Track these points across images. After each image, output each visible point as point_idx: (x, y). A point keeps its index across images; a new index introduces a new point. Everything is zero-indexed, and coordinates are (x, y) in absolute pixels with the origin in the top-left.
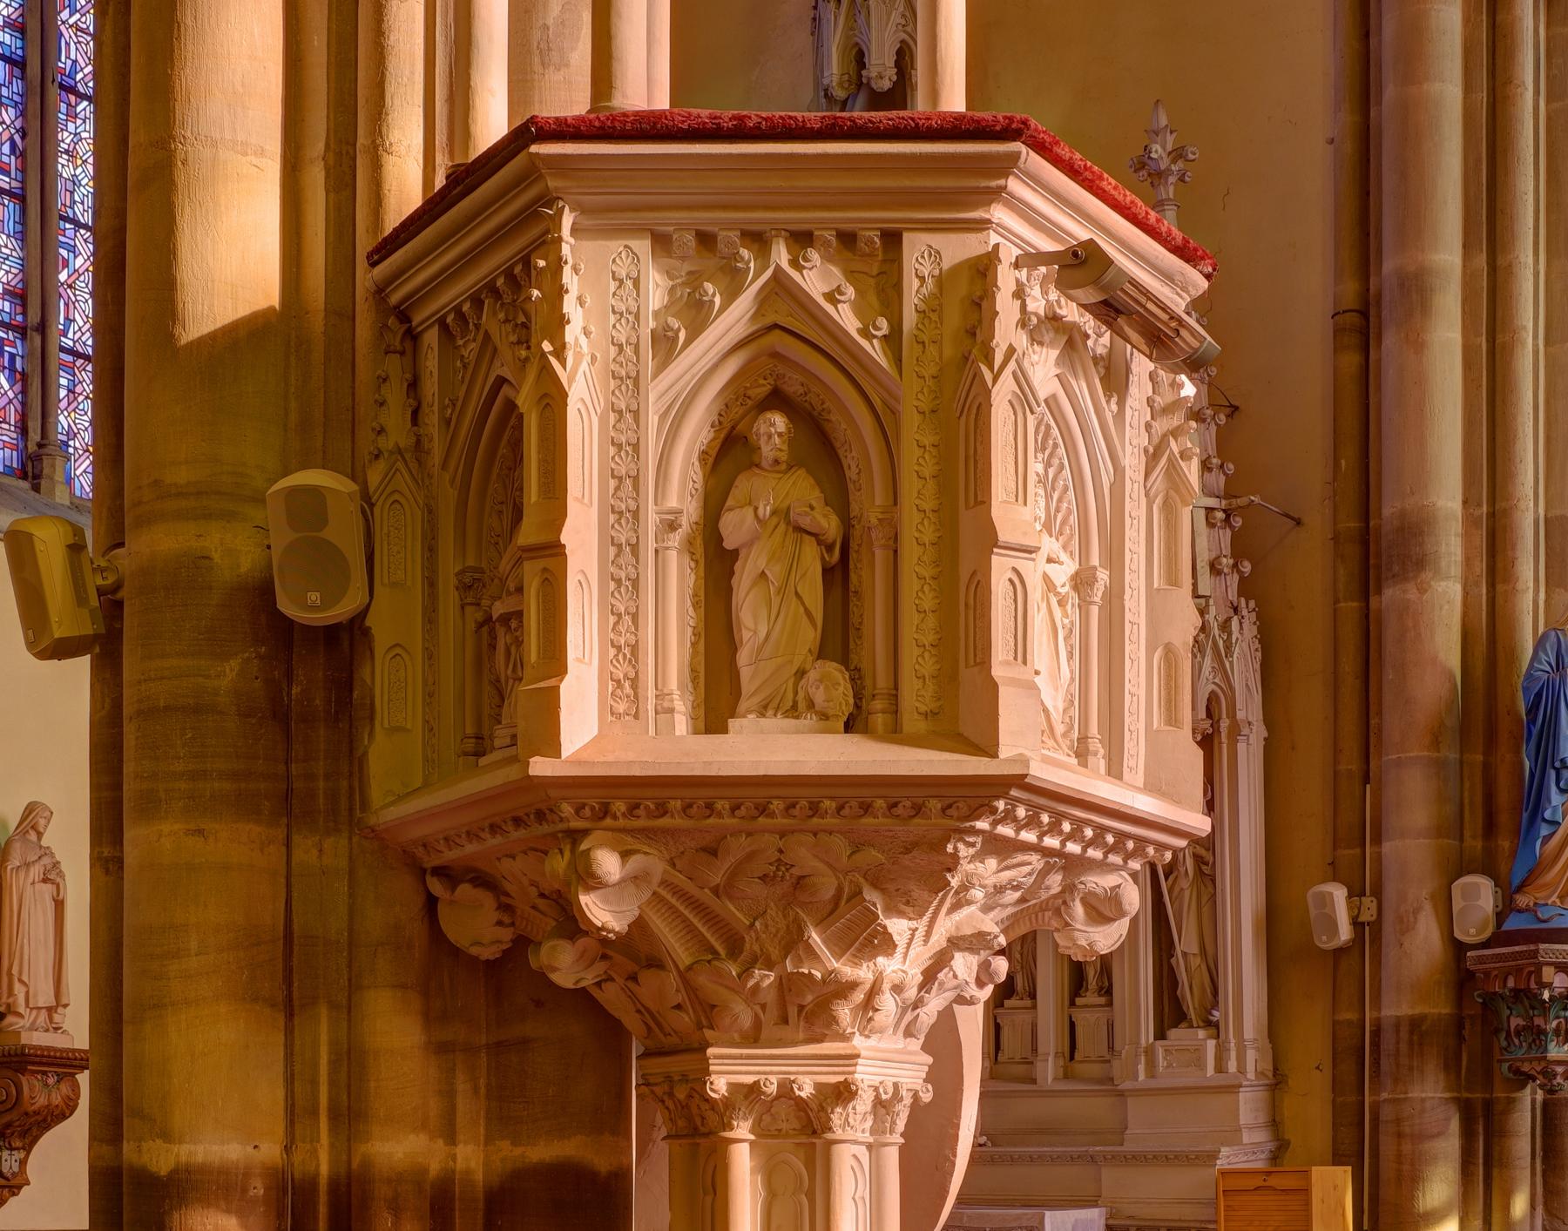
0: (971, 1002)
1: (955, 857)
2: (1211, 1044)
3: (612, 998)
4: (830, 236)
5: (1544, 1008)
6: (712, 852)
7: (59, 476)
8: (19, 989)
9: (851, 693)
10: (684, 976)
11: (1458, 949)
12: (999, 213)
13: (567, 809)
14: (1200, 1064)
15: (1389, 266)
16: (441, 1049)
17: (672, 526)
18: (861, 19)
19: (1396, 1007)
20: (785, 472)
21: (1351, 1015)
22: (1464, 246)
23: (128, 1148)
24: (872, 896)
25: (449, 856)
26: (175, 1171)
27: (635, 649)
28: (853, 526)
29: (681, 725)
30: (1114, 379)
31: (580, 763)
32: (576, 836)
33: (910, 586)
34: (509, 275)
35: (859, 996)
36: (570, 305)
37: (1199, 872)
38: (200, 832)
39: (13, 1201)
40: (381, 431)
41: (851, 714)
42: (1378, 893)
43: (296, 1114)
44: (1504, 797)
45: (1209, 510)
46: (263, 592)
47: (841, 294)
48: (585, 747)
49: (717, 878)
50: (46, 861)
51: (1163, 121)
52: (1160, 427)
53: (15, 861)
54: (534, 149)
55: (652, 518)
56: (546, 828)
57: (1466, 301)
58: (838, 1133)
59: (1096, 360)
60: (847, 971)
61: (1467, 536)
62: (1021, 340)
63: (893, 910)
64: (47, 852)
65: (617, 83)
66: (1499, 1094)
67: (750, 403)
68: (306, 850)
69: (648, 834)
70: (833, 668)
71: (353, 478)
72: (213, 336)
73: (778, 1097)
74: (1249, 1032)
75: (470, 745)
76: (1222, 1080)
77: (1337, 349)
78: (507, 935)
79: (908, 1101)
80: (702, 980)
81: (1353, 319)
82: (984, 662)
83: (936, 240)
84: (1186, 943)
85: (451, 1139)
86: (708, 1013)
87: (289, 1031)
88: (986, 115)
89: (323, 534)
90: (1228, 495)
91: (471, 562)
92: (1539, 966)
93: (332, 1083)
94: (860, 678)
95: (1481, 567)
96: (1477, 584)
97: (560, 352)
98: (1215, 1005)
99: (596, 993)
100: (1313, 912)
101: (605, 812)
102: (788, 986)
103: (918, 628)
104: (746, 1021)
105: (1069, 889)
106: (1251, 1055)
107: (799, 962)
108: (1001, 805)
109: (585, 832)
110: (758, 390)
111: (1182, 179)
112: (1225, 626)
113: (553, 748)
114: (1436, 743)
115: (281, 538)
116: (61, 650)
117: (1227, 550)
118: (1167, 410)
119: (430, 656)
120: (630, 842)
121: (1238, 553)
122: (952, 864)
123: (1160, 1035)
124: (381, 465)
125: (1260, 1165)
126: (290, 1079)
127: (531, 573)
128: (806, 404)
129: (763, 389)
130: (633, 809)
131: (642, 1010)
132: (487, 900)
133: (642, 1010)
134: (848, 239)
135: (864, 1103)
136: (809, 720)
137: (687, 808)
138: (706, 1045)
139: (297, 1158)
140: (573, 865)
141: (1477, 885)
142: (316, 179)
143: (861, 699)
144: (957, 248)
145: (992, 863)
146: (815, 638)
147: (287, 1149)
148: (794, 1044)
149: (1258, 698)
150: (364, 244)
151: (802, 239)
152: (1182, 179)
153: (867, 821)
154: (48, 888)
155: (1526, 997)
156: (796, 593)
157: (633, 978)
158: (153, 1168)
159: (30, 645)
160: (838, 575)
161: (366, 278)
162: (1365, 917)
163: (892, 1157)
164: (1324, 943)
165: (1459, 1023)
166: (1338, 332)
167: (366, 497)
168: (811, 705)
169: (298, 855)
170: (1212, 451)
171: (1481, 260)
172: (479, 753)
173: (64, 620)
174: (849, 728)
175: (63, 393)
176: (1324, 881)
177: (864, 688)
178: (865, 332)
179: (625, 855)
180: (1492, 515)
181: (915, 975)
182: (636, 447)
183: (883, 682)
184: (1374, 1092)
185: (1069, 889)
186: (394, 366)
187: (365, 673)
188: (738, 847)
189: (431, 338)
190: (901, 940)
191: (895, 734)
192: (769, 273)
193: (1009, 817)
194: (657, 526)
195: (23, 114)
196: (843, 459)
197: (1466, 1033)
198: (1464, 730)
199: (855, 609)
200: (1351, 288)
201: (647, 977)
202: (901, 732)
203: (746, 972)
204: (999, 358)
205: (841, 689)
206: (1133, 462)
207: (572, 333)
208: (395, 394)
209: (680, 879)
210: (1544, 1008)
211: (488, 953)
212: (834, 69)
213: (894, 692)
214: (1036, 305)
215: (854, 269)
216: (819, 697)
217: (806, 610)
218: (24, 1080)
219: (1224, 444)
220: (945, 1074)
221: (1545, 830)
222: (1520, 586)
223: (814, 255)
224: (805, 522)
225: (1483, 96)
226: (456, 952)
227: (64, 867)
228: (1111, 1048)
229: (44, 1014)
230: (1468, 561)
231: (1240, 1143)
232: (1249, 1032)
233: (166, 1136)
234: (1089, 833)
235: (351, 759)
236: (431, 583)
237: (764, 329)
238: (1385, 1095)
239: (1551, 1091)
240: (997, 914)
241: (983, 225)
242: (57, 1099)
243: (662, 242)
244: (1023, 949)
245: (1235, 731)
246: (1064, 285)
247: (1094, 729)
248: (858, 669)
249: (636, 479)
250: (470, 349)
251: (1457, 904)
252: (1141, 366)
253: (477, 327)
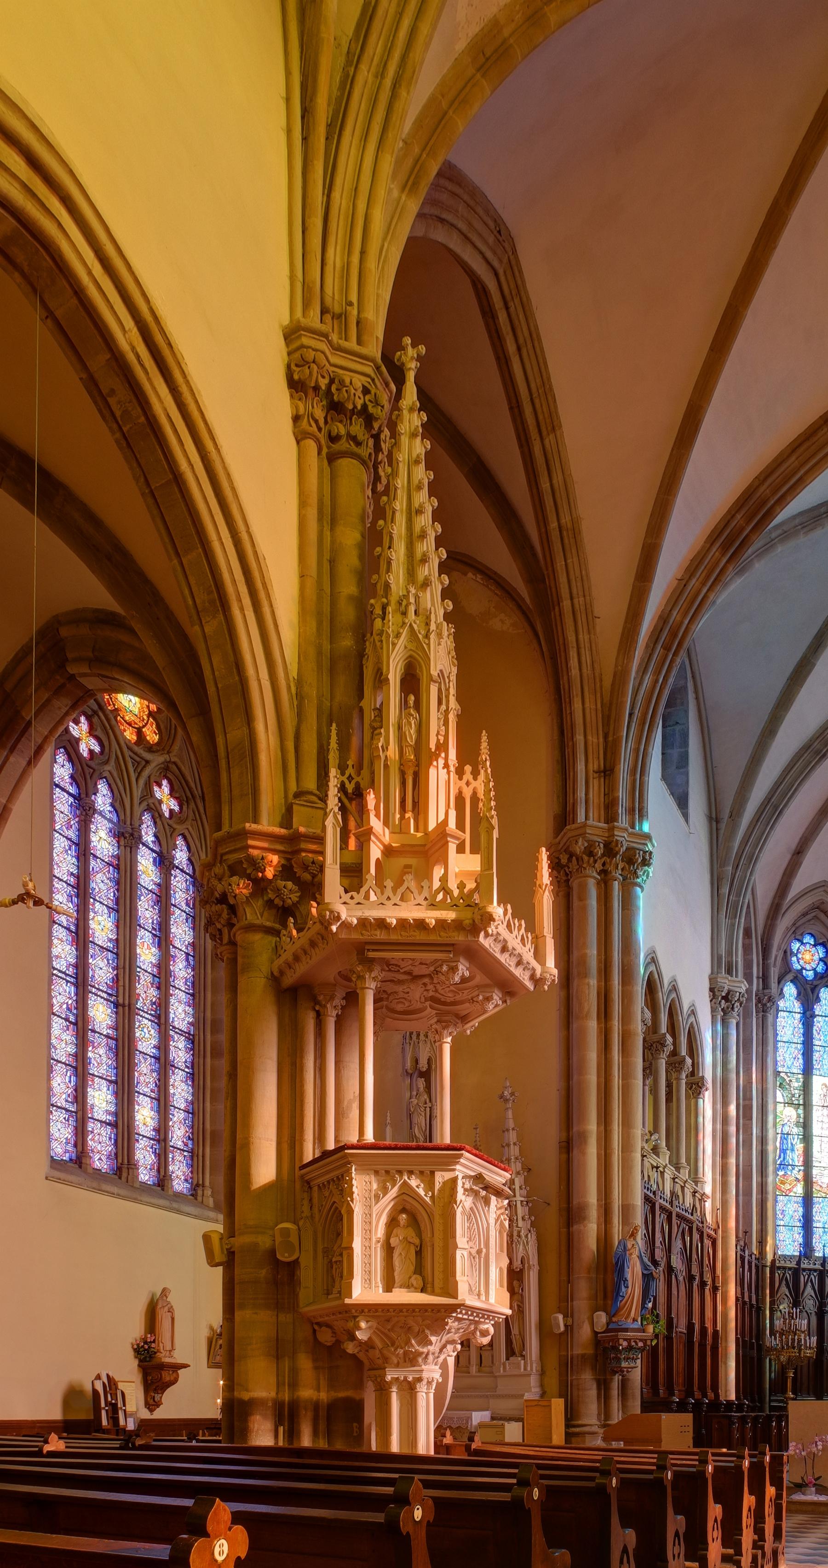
0: (451, 1356)
1: (448, 1322)
2: (522, 1362)
3: (361, 1356)
4: (418, 1172)
5: (620, 1352)
6: (388, 1321)
7: (170, 1186)
8: (161, 1345)
10: (380, 1351)
11: (596, 1333)
12: (458, 1167)
13: (353, 1311)
14: (519, 1368)
15: (575, 1129)
16: (316, 1368)
17: (379, 1242)
18: (417, 1049)
19: (578, 1351)
21: (564, 1353)
22: (598, 1123)
23: (235, 1393)
24: (427, 1332)
25: (320, 1320)
26: (249, 1400)
27: (370, 1272)
29: (381, 1290)
30: (487, 1202)
31: (357, 1300)
32: (355, 1317)
33: (436, 1257)
34: (338, 1177)
35: (424, 1356)
36: (354, 1189)
38: (256, 1313)
39: (158, 1409)
40: (303, 1212)
42: (572, 1316)
43: (279, 1385)
44: (609, 1288)
45: (522, 1201)
46: (272, 1253)
49: (389, 1327)
50: (169, 1305)
51: (508, 1084)
52: (499, 1212)
53: (160, 1306)
54: (346, 1151)
55: (374, 1240)
56: (347, 1315)
57: (598, 1140)
58: (418, 1390)
59: (482, 1197)
60: (421, 1350)
61: (598, 1210)
62: (463, 1198)
63: (432, 1335)
64: (169, 1303)
65: (365, 1133)
66: (608, 1377)
68: (282, 1317)
69: (373, 1317)
70: (419, 1277)
71: (294, 1223)
72: (260, 1188)
73: (403, 1381)
74: (534, 1358)
75: (326, 1292)
76: (526, 1372)
77: (560, 1153)
78: (334, 1339)
79: (435, 1381)
80: (385, 1352)
81: (564, 1144)
82: (454, 1237)
83: (443, 1173)
85: (319, 1391)
86: (386, 1360)
87: (277, 1364)
88: (455, 1144)
89: (290, 1239)
90: (527, 1197)
91: (326, 1246)
92: (619, 1339)
93: (289, 1377)
95: (602, 1219)
97: (352, 1200)
98: (524, 1350)
99: (357, 1355)
100: (553, 1322)
101: (363, 1311)
102: (406, 1353)
103: (438, 1268)
104: (396, 1361)
105: (476, 1329)
106: (534, 1365)
107: (409, 1348)
108: (459, 1310)
109: (358, 1316)
111: (514, 1101)
112: (526, 1236)
113: (350, 1297)
114: (589, 1272)
115: (278, 1240)
116: (217, 1265)
117: (527, 1214)
118: (500, 1208)
119: (315, 1269)
120: (369, 1319)
121: (530, 1215)
122: (447, 1324)
123: (507, 1359)
124: (303, 1220)
125: (537, 1398)
126: (278, 1376)
127: (345, 1253)
129: (401, 1207)
130: (369, 1311)
131: (369, 1359)
132: (329, 1331)
133: (369, 1359)
134: (422, 1173)
135: (425, 1382)
136: (412, 1289)
137: (383, 1310)
138: (385, 1368)
139: (280, 1396)
140: (354, 1324)
141: (601, 1315)
142: (285, 1146)
144: (448, 1175)
145: (456, 1323)
148: (407, 1367)
149: (536, 1257)
150: (298, 1165)
151: (411, 1173)
152: (514, 1101)
153: (426, 1314)
154: (170, 1313)
155: (615, 1348)
157: (367, 1351)
158: (244, 1398)
159: (209, 1263)
160: (419, 1253)
161: (298, 1173)
163: (431, 1396)
164: (556, 1331)
165: (596, 1356)
166: (560, 1148)
167: (299, 1229)
168: (413, 1285)
169: (280, 1318)
170: (523, 1183)
171: (602, 1128)
172: (328, 1294)
173: (219, 1257)
174: (422, 1291)
175: (170, 1159)
176: (557, 1313)
178: (426, 1195)
179: (367, 1322)
180: (605, 1204)
181: (438, 1350)
182: (370, 1223)
183: (430, 1279)
184: (572, 1376)
185: (476, 1329)
186: (306, 1195)
187: (298, 1273)
188: (395, 1319)
189: (316, 1189)
190: (434, 1342)
191: (433, 1293)
193: (461, 1313)
195: (159, 1074)
197: (598, 1358)
200: (564, 1134)
201: (370, 1350)
203: (396, 1349)
204: (458, 1203)
206: (492, 1221)
207: (355, 1196)
208: (306, 1202)
209: (380, 1327)
210: (620, 1352)
211: (329, 1344)
212: (409, 1064)
214: (467, 1186)
216: (415, 1283)
218: (163, 1372)
219: (526, 1181)
220: (445, 1375)
221: (620, 1299)
222: (614, 1225)
223: (413, 1176)
224: (411, 1241)
225: (603, 1080)
226: (320, 1343)
227: (174, 1307)
228: (493, 1362)
229: (168, 1352)
230: (598, 1218)
231: (531, 1391)
232: (534, 1358)
233: (247, 1390)
234: (481, 1315)
235: (294, 1295)
236: (315, 1251)
237: (401, 1194)
238: (574, 1377)
239: (623, 1376)
240: (457, 1335)
241: (454, 1170)
242: (172, 1378)
243: (376, 1173)
244: (466, 1344)
245: (529, 1267)
246: (475, 1183)
250: (327, 1194)
251: (595, 1320)
252: (493, 1198)
253: (329, 1188)
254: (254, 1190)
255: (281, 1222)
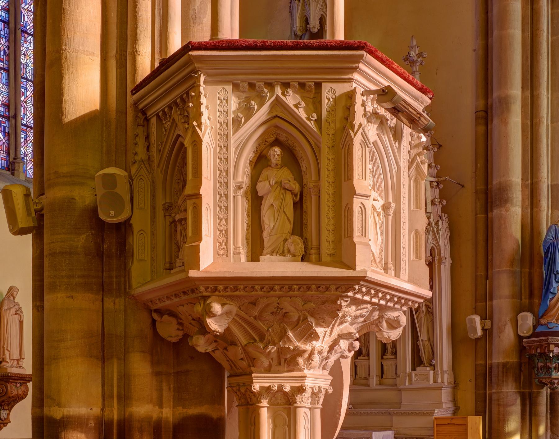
0: (346, 357)
1: (341, 306)
2: (432, 372)
3: (218, 356)
4: (296, 84)
5: (550, 359)
6: (254, 304)
7: (21, 170)
8: (7, 353)
9: (303, 247)
10: (244, 348)
11: (520, 338)
12: (356, 76)
13: (202, 289)
14: (428, 379)
15: (495, 95)
16: (157, 374)
17: (240, 188)
18: (307, 7)
19: (498, 359)
20: (280, 168)
21: (481, 362)
22: (522, 88)
23: (45, 409)
24: (311, 320)
25: (160, 305)
26: (62, 418)
27: (226, 231)
28: (304, 188)
29: (243, 258)
30: (397, 135)
31: (207, 272)
32: (205, 298)
33: (324, 209)
34: (182, 98)
35: (306, 355)
36: (203, 109)
37: (428, 311)
38: (71, 297)
39: (5, 428)
40: (136, 154)
41: (303, 255)
42: (491, 318)
43: (105, 397)
44: (536, 284)
45: (431, 182)
46: (94, 211)
47: (300, 105)
48: (208, 267)
49: (256, 313)
50: (16, 307)
51: (415, 43)
52: (414, 152)
53: (5, 307)
54: (190, 53)
55: (232, 185)
56: (195, 295)
57: (523, 107)
58: (299, 404)
59: (391, 128)
60: (302, 346)
61: (523, 191)
62: (364, 121)
63: (318, 325)
64: (17, 304)
65: (220, 30)
66: (535, 390)
67: (267, 144)
68: (109, 303)
69: (231, 297)
70: (297, 238)
71: (126, 171)
72: (76, 120)
73: (277, 391)
74: (445, 368)
75: (168, 266)
76: (435, 385)
77: (477, 124)
78: (181, 333)
79: (324, 393)
80: (250, 349)
81: (482, 114)
82: (351, 236)
83: (334, 86)
84: (423, 336)
85: (161, 406)
86: (252, 361)
87: (103, 368)
88: (351, 41)
89: (115, 191)
90: (438, 177)
91: (168, 200)
92: (549, 345)
93: (118, 386)
94: (307, 242)
95: (528, 202)
96: (527, 208)
97: (200, 126)
98: (433, 358)
99: (212, 354)
100: (468, 325)
101: (216, 289)
102: (281, 352)
103: (327, 224)
104: (266, 364)
105: (381, 317)
106: (446, 376)
107: (285, 343)
108: (357, 287)
109: (209, 297)
110: (270, 139)
111: (421, 64)
112: (437, 223)
113: (197, 267)
114: (512, 265)
115: (100, 192)
116: (22, 232)
117: (437, 196)
118: (416, 146)
119: (153, 234)
120: (225, 300)
121: (441, 197)
122: (340, 308)
123: (414, 369)
124: (136, 166)
125: (449, 416)
126: (103, 385)
127: (189, 204)
128: (287, 144)
129: (272, 139)
130: (226, 288)
131: (229, 360)
132: (174, 321)
133: (229, 360)
134: (302, 85)
135: (308, 393)
136: (289, 257)
137: (245, 288)
138: (252, 373)
139: (106, 413)
140: (204, 308)
141: (526, 316)
142: (113, 64)
143: (307, 249)
144: (341, 89)
145: (354, 308)
146: (291, 227)
147: (102, 410)
148: (283, 372)
149: (448, 249)
150: (130, 87)
151: (286, 85)
152: (421, 64)
153: (309, 293)
154: (17, 317)
155: (544, 356)
156: (284, 212)
157: (226, 349)
158: (55, 417)
159: (11, 230)
160: (299, 205)
161: (130, 99)
162: (487, 327)
163: (318, 413)
164: (472, 336)
165: (520, 365)
166: (477, 118)
167: (131, 177)
168: (289, 251)
169: (106, 305)
170: (432, 161)
171: (528, 93)
172: (171, 269)
173: (23, 221)
174: (303, 259)
175: (22, 140)
176: (472, 314)
177: (308, 245)
178: (308, 119)
179: (223, 305)
180: (532, 184)
181: (326, 348)
182: (227, 159)
183: (315, 243)
184: (490, 389)
185: (381, 317)
186: (140, 131)
187: (130, 240)
188: (263, 302)
189: (154, 120)
190: (321, 335)
191: (319, 262)
192: (274, 97)
193: (360, 291)
194: (234, 188)
195: (8, 41)
196: (300, 164)
197: (523, 368)
198: (522, 260)
199: (305, 217)
200: (482, 103)
201: (231, 348)
202: (321, 261)
203: (266, 347)
204: (356, 128)
205: (300, 246)
206: (404, 165)
207: (204, 119)
208: (141, 141)
209: (243, 314)
210: (550, 359)
211: (174, 340)
212: (297, 25)
213: (319, 247)
214: (369, 109)
215: (304, 96)
216: (292, 249)
217: (287, 217)
218: (9, 385)
219: (436, 158)
220: (337, 383)
221: (551, 296)
222: (542, 209)
223: (290, 91)
224: (287, 186)
225: (529, 34)
226: (162, 340)
227: (23, 309)
228: (396, 374)
229: (16, 362)
230: (523, 200)
231: (442, 408)
232: (445, 368)
233: (59, 405)
234: (388, 297)
235: (125, 271)
236: (154, 208)
237: (272, 117)
238: (494, 391)
239: (553, 389)
240: (356, 326)
241: (350, 80)
242: (20, 392)
243: (236, 86)
244: (365, 338)
245: (440, 261)
246: (379, 102)
247: (390, 260)
248: (306, 239)
249: (227, 171)
250: (168, 125)
251: (520, 322)
252: (407, 131)
253: (170, 116)
254: (71, 122)
255: (109, 166)
